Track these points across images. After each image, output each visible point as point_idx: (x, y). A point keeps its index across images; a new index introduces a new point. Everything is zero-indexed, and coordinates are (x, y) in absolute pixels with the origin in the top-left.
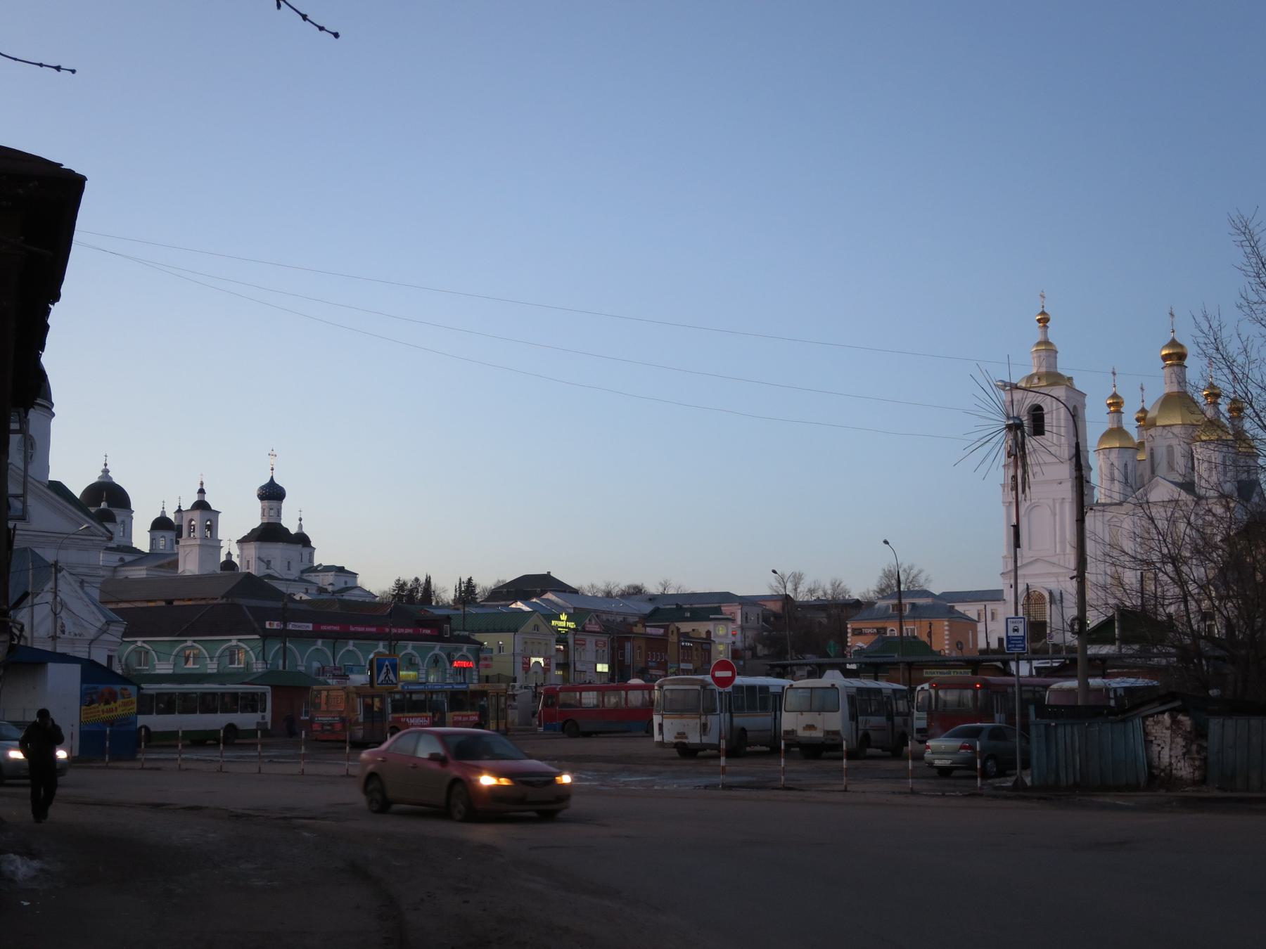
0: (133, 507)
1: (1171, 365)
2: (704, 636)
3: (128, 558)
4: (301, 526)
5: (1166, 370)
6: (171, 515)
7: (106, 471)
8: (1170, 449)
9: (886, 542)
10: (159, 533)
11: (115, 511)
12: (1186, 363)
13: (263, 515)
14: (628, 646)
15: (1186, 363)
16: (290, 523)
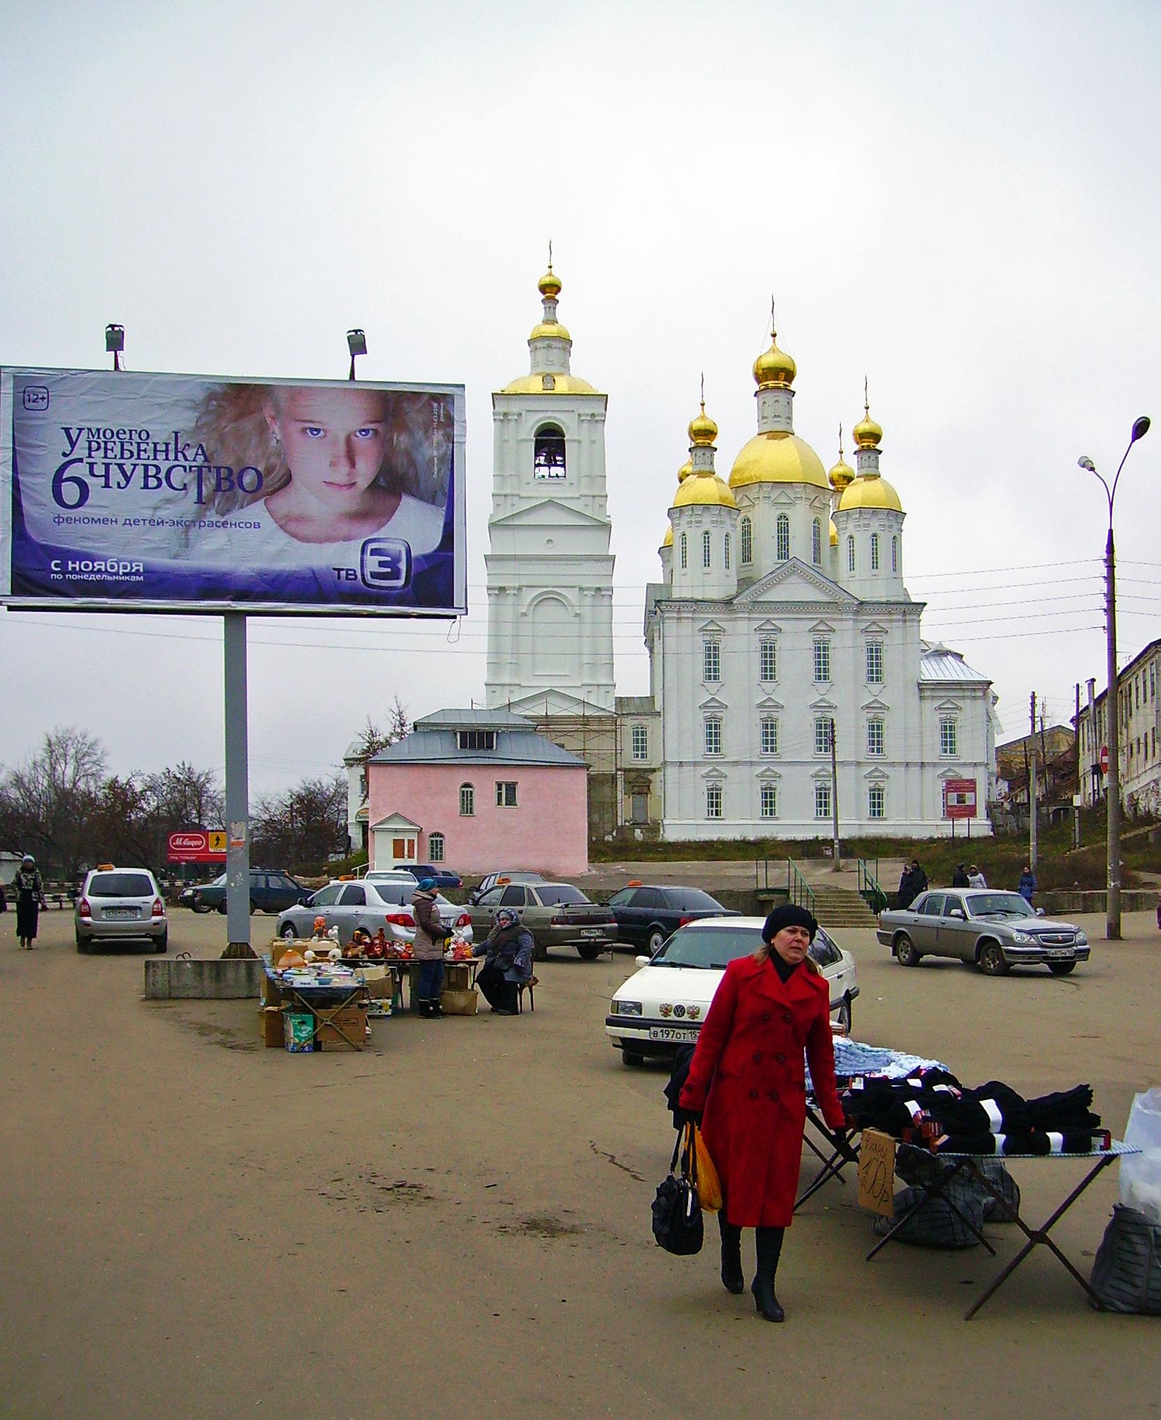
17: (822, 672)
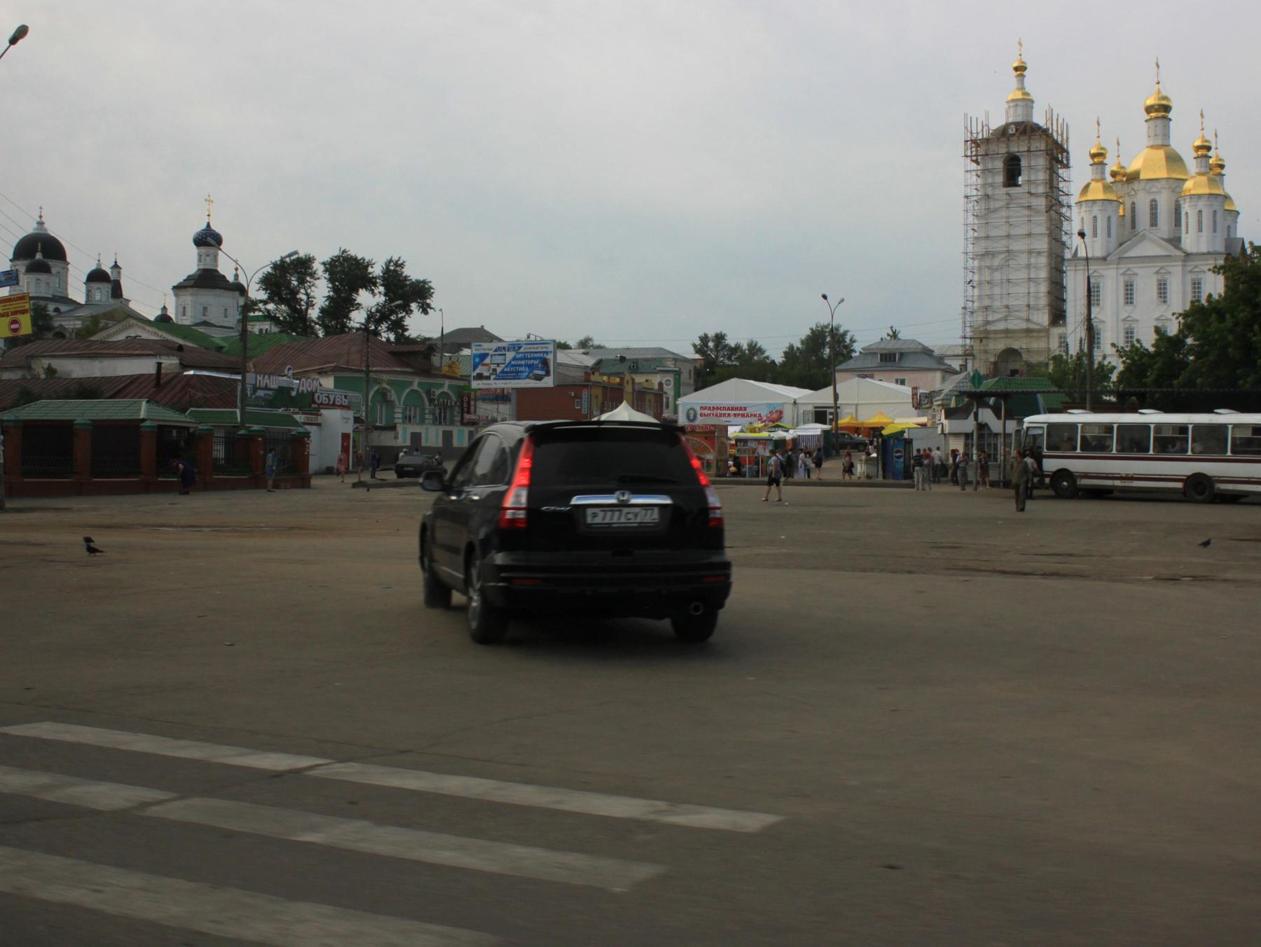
0: (68, 259)
1: (1156, 118)
2: (656, 387)
3: (63, 308)
4: (236, 276)
5: (1152, 123)
6: (107, 268)
7: (41, 224)
8: (1154, 207)
9: (825, 297)
10: (94, 285)
11: (51, 263)
12: (1170, 115)
13: (200, 260)
14: (585, 394)
15: (1170, 115)
16: (226, 269)
17: (1129, 298)
